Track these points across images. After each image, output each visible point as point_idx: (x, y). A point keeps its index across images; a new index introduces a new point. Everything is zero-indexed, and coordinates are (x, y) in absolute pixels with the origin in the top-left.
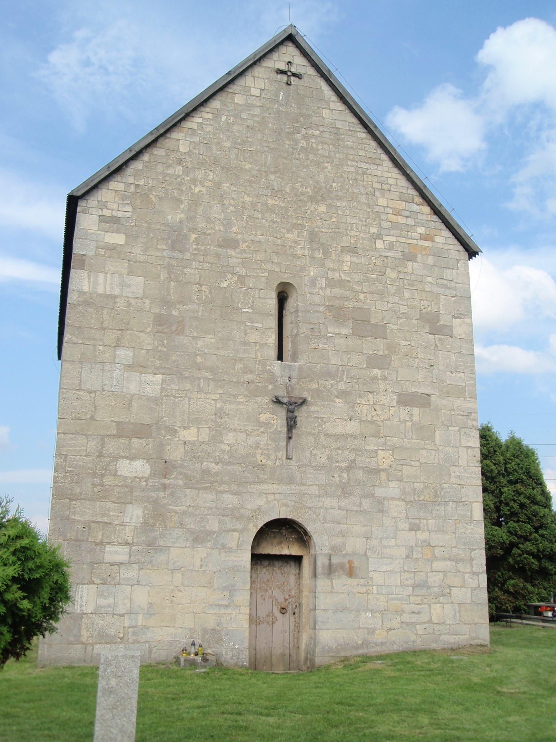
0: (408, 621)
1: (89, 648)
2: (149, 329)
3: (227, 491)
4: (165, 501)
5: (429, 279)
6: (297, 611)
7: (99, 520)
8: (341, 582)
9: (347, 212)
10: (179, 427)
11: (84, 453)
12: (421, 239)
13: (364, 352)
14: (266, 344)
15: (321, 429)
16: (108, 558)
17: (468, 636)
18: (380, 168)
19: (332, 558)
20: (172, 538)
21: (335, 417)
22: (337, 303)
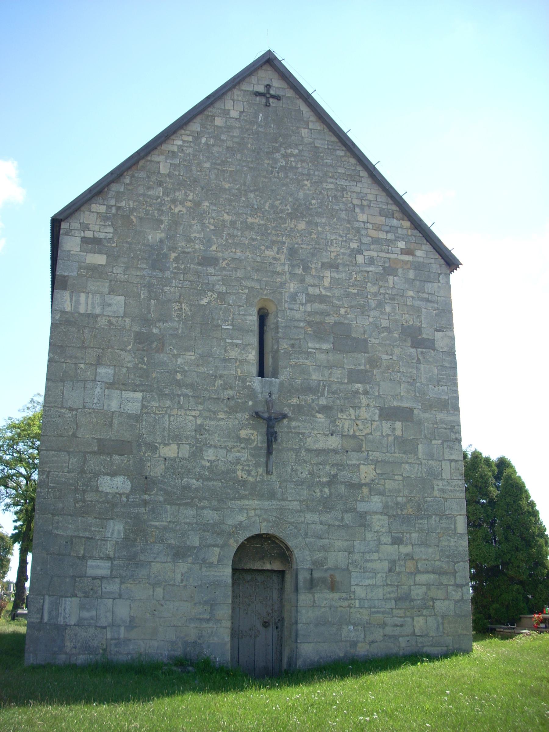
0: (390, 634)
2: (130, 347)
3: (207, 507)
4: (145, 517)
5: (411, 293)
6: (279, 624)
7: (81, 535)
8: (325, 597)
9: (327, 228)
13: (345, 366)
18: (359, 185)
19: (313, 573)
20: (153, 553)
22: (318, 319)
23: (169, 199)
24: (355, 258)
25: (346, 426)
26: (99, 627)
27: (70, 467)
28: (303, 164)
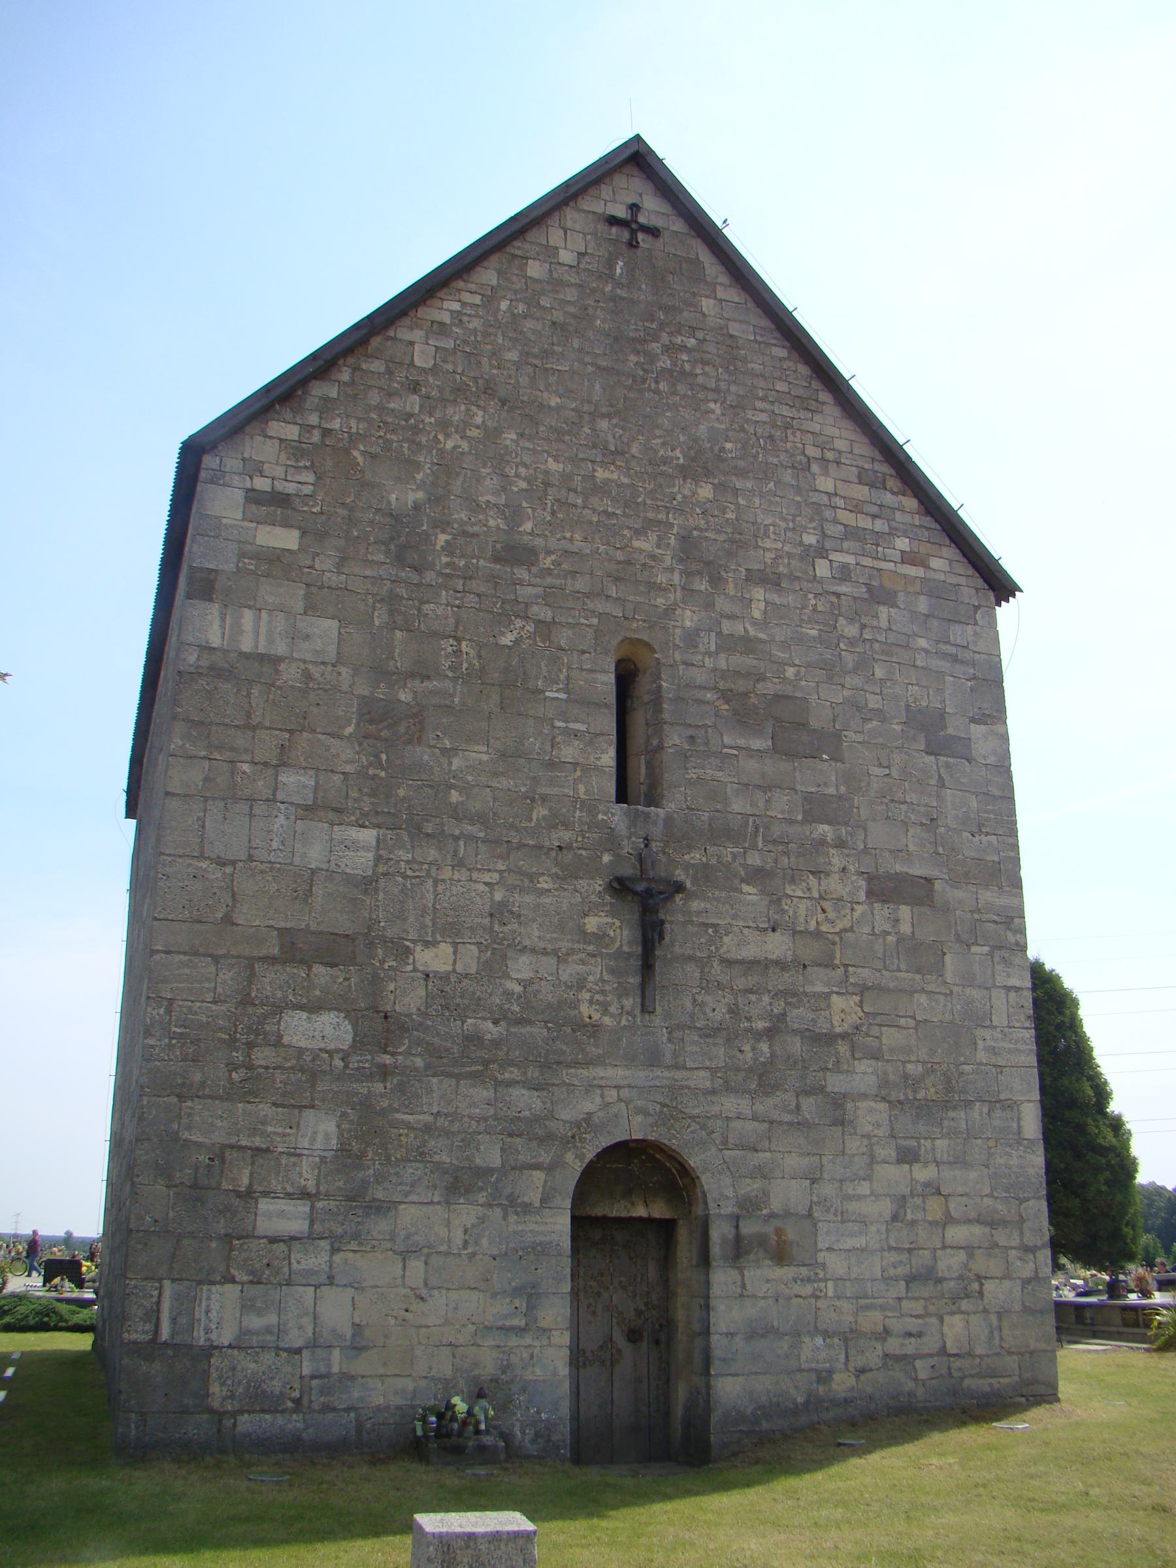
0: (897, 1352)
1: (228, 1423)
2: (349, 730)
4: (385, 1103)
5: (922, 643)
7: (243, 1143)
8: (763, 1276)
9: (757, 501)
10: (414, 942)
11: (209, 997)
12: (903, 562)
13: (798, 787)
14: (597, 769)
15: (713, 948)
16: (265, 1226)
17: (1016, 1378)
18: (817, 417)
19: (741, 1224)
21: (741, 923)
22: (741, 685)
27: (220, 990)
28: (707, 368)
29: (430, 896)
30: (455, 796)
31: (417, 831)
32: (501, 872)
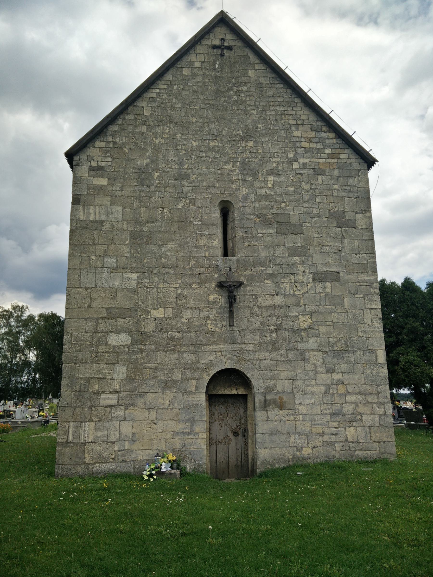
1: (91, 467)
2: (127, 242)
5: (336, 187)
7: (96, 377)
8: (275, 413)
9: (270, 144)
11: (84, 331)
13: (286, 245)
16: (103, 402)
18: (295, 109)
20: (148, 387)
21: (265, 294)
22: (264, 211)
23: (151, 133)
24: (292, 165)
25: (288, 288)
26: (110, 442)
27: (87, 329)
28: (251, 98)
29: (156, 293)
30: (163, 260)
31: (150, 272)
32: (179, 283)
